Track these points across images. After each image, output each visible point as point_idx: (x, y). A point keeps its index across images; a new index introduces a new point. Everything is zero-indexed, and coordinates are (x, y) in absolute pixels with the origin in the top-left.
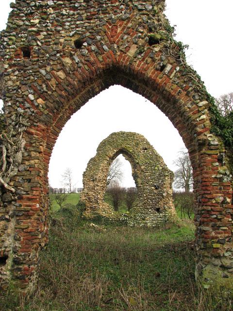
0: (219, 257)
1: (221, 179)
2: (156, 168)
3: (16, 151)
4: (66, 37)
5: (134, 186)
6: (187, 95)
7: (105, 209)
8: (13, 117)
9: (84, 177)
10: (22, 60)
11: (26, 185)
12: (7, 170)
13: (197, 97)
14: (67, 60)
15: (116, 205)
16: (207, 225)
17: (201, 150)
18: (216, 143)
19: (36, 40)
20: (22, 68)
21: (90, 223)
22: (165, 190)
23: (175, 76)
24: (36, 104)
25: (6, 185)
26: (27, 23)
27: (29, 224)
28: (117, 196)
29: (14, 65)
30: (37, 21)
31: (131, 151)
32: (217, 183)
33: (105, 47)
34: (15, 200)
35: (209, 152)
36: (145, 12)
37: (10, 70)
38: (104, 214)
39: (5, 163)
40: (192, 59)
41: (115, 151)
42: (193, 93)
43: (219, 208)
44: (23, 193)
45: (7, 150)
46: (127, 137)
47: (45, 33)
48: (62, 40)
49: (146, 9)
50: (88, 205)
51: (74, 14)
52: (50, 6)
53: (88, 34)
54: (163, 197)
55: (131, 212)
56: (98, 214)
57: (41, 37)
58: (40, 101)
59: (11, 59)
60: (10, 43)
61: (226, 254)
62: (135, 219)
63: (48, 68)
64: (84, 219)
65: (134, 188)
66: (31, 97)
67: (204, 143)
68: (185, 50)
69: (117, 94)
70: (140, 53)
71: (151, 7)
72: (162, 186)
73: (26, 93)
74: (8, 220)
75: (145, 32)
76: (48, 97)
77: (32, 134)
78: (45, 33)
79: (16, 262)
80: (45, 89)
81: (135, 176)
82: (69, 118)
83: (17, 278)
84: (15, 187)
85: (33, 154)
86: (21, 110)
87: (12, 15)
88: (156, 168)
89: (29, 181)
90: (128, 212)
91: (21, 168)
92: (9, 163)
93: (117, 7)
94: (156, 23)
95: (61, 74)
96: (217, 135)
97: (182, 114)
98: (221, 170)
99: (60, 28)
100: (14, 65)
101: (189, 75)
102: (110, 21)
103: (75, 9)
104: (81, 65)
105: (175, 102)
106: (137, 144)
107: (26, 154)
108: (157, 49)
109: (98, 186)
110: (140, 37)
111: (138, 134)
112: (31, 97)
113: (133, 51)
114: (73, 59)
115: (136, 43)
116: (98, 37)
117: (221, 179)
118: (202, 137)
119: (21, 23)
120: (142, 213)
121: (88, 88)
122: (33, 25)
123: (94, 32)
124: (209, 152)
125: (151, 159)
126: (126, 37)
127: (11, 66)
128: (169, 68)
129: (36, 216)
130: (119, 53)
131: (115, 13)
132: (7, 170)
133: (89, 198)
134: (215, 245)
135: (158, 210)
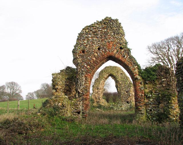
0: (140, 111)
1: (141, 89)
2: (127, 83)
3: (82, 82)
4: (96, 47)
5: (116, 91)
6: (131, 64)
7: (103, 102)
8: (81, 72)
9: (93, 88)
10: (82, 54)
11: (85, 91)
12: (80, 87)
13: (134, 65)
14: (96, 54)
15: (108, 101)
16: (137, 102)
17: (136, 80)
18: (139, 78)
19: (86, 48)
20: (82, 56)
21: (96, 108)
22: (131, 93)
23: (128, 59)
24: (87, 68)
25: (80, 91)
26: (83, 42)
27: (85, 102)
28: (108, 96)
29: (80, 56)
30: (86, 42)
31: (115, 75)
32: (140, 90)
33: (107, 50)
34: (82, 96)
35: (138, 81)
36: (118, 39)
37: (79, 57)
38: (103, 104)
39: (79, 85)
40: (133, 54)
41: (107, 75)
42: (133, 64)
43: (140, 97)
44: (85, 93)
45: (80, 81)
46: (113, 68)
47: (89, 46)
48: (94, 48)
49: (119, 38)
50: (95, 100)
51: (97, 40)
52: (90, 37)
53: (102, 46)
54: (130, 96)
55: (115, 103)
56: (100, 104)
57: (88, 47)
58: (88, 67)
59: (79, 54)
60: (78, 49)
61: (142, 110)
62: (117, 107)
63: (90, 57)
64: (94, 107)
65: (116, 93)
66: (86, 66)
67: (137, 78)
68: (131, 50)
69: (111, 63)
70: (117, 52)
71: (120, 37)
72: (129, 91)
73: (84, 64)
74: (80, 101)
75: (119, 45)
76: (91, 66)
77: (86, 76)
78: (89, 46)
79: (83, 113)
80: (90, 63)
81: (117, 87)
82: (75, 46)
83: (84, 117)
84: (82, 92)
85: (87, 82)
86: (83, 70)
87: (78, 39)
88: (127, 83)
89: (86, 90)
90: (114, 103)
91: (84, 86)
92: (80, 85)
93: (110, 37)
94: (122, 42)
95: (94, 59)
96: (140, 76)
97: (130, 70)
98: (141, 86)
99: (93, 44)
100: (80, 56)
101: (132, 58)
102: (109, 42)
103: (97, 38)
104: (100, 56)
105: (128, 67)
106: (117, 72)
107: (85, 82)
108: (122, 51)
109: (99, 91)
110: (117, 47)
111: (118, 67)
112: (86, 66)
113: (115, 51)
114: (97, 54)
115: (116, 49)
116: (105, 47)
117: (141, 89)
118: (135, 77)
119: (81, 42)
120: (120, 104)
121: (102, 62)
122: (85, 43)
123: (104, 45)
124: (138, 81)
125: (124, 78)
126: (113, 47)
127: (79, 56)
128: (126, 56)
129: (88, 100)
130: (111, 52)
131: (110, 39)
132: (80, 87)
133: (96, 97)
134: (139, 107)
135: (128, 102)
